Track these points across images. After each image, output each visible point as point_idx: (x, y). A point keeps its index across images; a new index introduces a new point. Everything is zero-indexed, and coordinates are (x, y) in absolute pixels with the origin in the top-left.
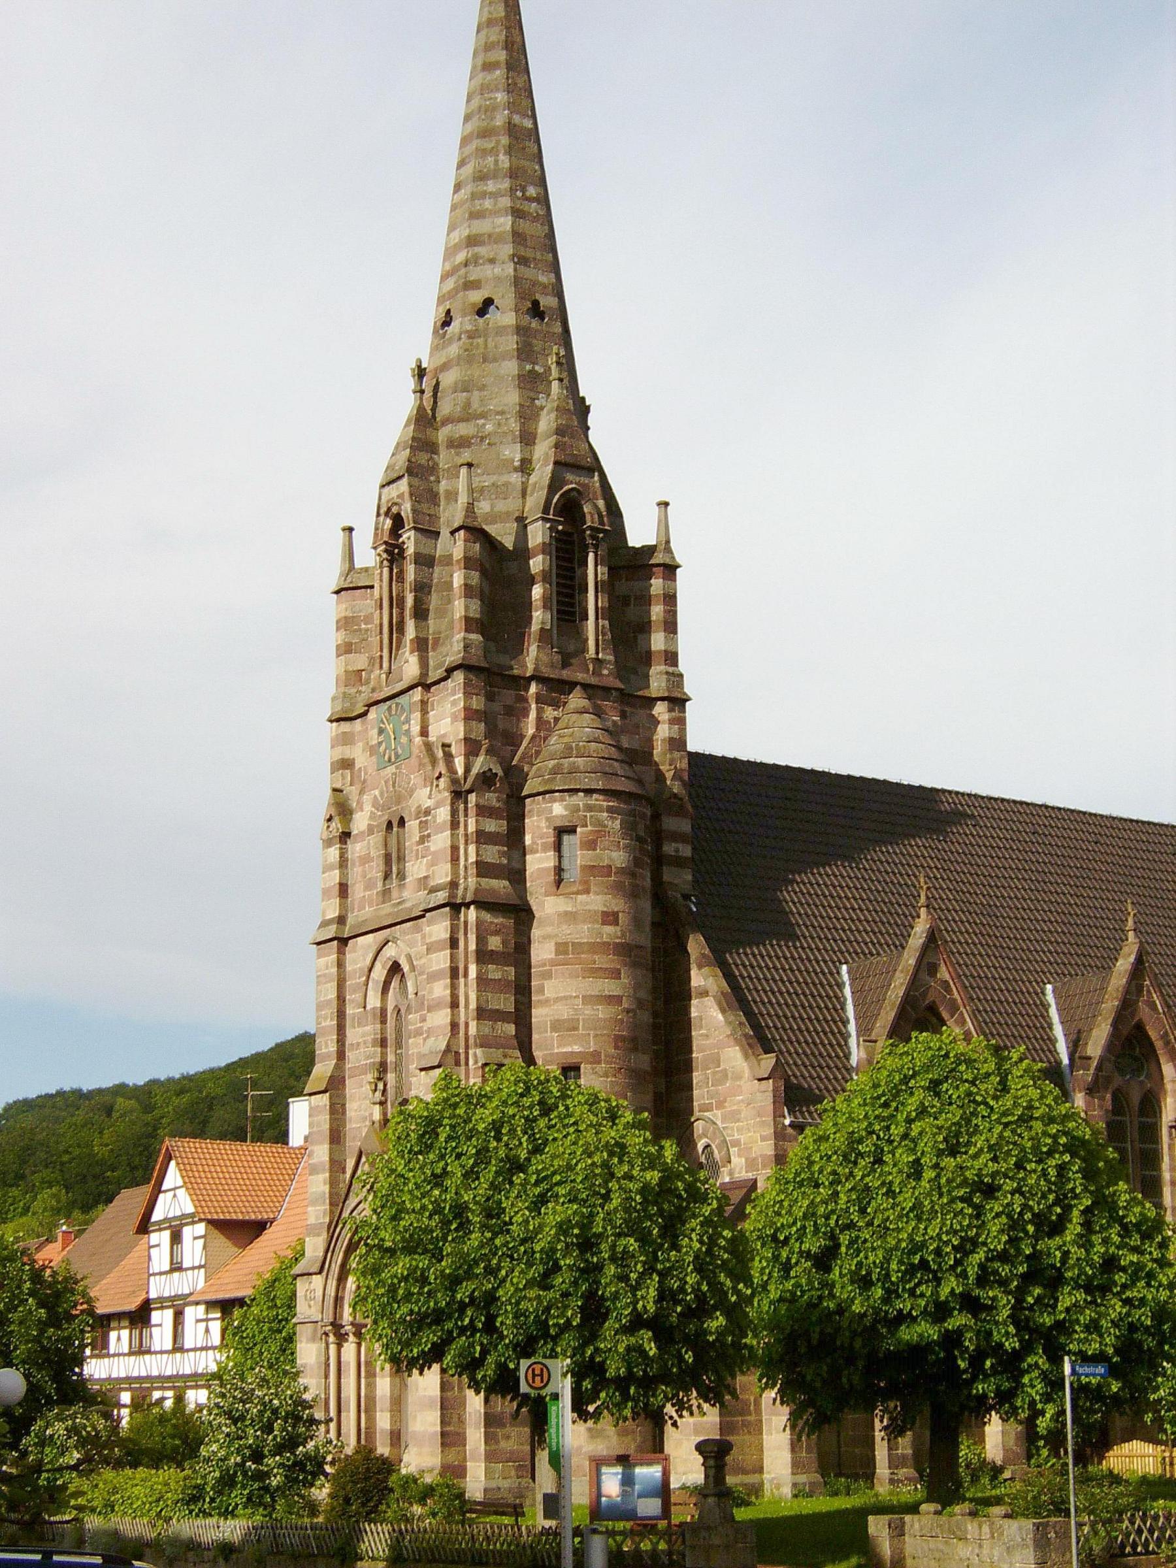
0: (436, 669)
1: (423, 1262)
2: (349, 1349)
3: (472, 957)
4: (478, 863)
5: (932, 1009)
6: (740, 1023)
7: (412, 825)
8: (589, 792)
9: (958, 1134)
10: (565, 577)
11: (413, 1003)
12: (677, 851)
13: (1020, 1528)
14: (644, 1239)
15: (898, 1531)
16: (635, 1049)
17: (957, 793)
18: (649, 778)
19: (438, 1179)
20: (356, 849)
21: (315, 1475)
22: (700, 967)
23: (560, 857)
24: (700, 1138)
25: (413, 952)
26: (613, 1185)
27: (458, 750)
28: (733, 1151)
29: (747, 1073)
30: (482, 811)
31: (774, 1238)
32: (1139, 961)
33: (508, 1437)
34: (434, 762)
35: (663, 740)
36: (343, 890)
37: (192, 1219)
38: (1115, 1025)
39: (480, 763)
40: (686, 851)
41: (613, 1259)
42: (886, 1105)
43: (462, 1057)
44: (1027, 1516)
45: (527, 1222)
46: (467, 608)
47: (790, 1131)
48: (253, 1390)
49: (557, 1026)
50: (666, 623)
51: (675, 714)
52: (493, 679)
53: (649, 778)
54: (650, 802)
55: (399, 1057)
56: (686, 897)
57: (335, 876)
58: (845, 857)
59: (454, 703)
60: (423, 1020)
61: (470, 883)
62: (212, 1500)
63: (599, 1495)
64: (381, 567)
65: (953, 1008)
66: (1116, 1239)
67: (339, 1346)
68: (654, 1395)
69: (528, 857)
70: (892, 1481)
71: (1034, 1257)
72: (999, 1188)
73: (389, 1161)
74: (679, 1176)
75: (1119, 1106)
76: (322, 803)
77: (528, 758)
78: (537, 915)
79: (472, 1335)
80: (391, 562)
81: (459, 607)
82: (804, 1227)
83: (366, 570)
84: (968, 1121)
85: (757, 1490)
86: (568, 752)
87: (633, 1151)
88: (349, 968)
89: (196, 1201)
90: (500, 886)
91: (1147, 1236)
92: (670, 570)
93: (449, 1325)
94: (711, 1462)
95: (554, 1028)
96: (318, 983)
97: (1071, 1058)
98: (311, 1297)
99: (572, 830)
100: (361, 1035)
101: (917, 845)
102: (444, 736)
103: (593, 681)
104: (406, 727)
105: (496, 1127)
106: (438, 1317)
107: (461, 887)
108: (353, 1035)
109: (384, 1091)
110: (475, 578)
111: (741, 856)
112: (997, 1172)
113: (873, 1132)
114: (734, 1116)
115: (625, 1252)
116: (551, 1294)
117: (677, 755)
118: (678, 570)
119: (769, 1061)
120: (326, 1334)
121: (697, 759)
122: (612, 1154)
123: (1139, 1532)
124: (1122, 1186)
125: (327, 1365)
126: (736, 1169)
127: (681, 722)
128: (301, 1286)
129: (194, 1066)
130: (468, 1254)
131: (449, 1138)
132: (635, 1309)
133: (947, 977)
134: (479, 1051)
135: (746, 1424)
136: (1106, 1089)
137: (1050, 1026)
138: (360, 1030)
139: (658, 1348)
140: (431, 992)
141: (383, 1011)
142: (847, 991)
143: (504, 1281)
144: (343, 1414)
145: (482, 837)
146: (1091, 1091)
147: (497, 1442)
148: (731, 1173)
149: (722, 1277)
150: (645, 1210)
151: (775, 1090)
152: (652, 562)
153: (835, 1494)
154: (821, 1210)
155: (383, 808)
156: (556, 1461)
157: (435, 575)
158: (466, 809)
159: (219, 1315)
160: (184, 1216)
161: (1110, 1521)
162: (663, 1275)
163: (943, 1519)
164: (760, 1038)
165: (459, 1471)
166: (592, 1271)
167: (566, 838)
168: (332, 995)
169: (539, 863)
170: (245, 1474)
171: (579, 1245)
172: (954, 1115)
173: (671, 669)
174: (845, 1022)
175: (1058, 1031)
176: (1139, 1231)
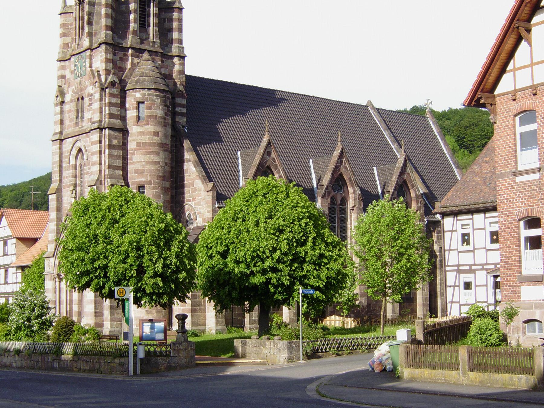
0: (95, 43)
1: (82, 254)
2: (63, 284)
3: (107, 147)
4: (109, 114)
5: (269, 168)
6: (201, 172)
7: (86, 99)
8: (149, 89)
9: (272, 212)
10: (142, 11)
11: (86, 163)
12: (181, 110)
13: (283, 344)
14: (158, 246)
15: (244, 345)
16: (164, 180)
17: (282, 91)
18: (171, 84)
19: (88, 226)
20: (66, 107)
21: (49, 326)
22: (188, 152)
23: (139, 112)
24: (187, 211)
25: (86, 145)
26: (148, 228)
27: (103, 73)
28: (198, 216)
29: (203, 189)
30: (111, 95)
31: (207, 247)
32: (342, 152)
33: (118, 314)
34: (94, 77)
35: (177, 71)
36: (62, 122)
37: (11, 237)
38: (332, 174)
39: (110, 78)
40: (184, 110)
41: (148, 253)
42: (247, 201)
43: (103, 182)
44: (286, 340)
45: (118, 241)
46: (106, 22)
47: (217, 209)
48: (27, 297)
49: (137, 171)
50: (178, 29)
51: (181, 62)
52: (116, 47)
53: (171, 84)
54: (171, 93)
55: (81, 181)
56: (184, 127)
57: (59, 117)
58: (240, 114)
59: (101, 56)
60: (89, 169)
61: (106, 121)
62: (14, 335)
63: (143, 332)
64: (76, 6)
65: (276, 167)
66: (323, 248)
67: (60, 282)
68: (162, 299)
69: (127, 112)
70: (250, 328)
71: (296, 254)
72: (285, 230)
73: (72, 219)
74: (171, 225)
75: (333, 202)
76: (54, 91)
77: (128, 76)
78: (130, 132)
79: (100, 278)
80: (80, 4)
81: (103, 22)
82: (217, 243)
83: (71, 6)
84: (275, 207)
85: (204, 331)
86: (142, 75)
87: (155, 217)
88: (64, 150)
89: (13, 231)
90: (117, 122)
91: (334, 247)
92: (180, 9)
93: (92, 275)
94: (181, 322)
95: (136, 172)
96: (53, 155)
97: (317, 186)
98: (51, 266)
99: (143, 103)
100: (68, 173)
101: (266, 110)
102: (98, 68)
103: (152, 49)
104: (84, 64)
105: (109, 208)
106: (88, 273)
107: (103, 122)
108: (64, 174)
109: (76, 194)
110: (110, 10)
111: (203, 111)
112: (284, 225)
113: (242, 211)
114: (198, 204)
115: (151, 251)
116: (127, 266)
117: (181, 76)
118: (183, 10)
119: (211, 185)
120: (55, 278)
121: (189, 78)
122: (148, 218)
123: (324, 345)
124: (327, 230)
125: (56, 289)
126: (199, 222)
127: (183, 64)
128: (46, 262)
129: (17, 181)
130: (98, 252)
131: (93, 211)
132: (155, 270)
133: (274, 156)
134: (109, 180)
135: (200, 309)
136: (329, 196)
137: (311, 174)
138: (67, 172)
139: (163, 284)
140: (92, 159)
141: (76, 165)
142: (240, 161)
143: (110, 261)
144: (61, 306)
145: (111, 104)
146: (323, 197)
147: (114, 315)
148: (197, 224)
149: (185, 260)
150: (159, 237)
151: (213, 195)
152: (174, 7)
153: (231, 333)
154: (223, 238)
155: (76, 93)
156: (128, 321)
157: (96, 9)
158: (105, 94)
159: (21, 271)
160: (8, 236)
161: (314, 341)
162: (165, 259)
163: (259, 340)
164: (208, 177)
165: (101, 325)
166: (140, 257)
167: (141, 105)
168: (58, 159)
169: (131, 114)
170: (25, 326)
171: (136, 248)
172: (271, 205)
173: (180, 46)
174: (238, 172)
175: (313, 176)
176: (332, 245)
